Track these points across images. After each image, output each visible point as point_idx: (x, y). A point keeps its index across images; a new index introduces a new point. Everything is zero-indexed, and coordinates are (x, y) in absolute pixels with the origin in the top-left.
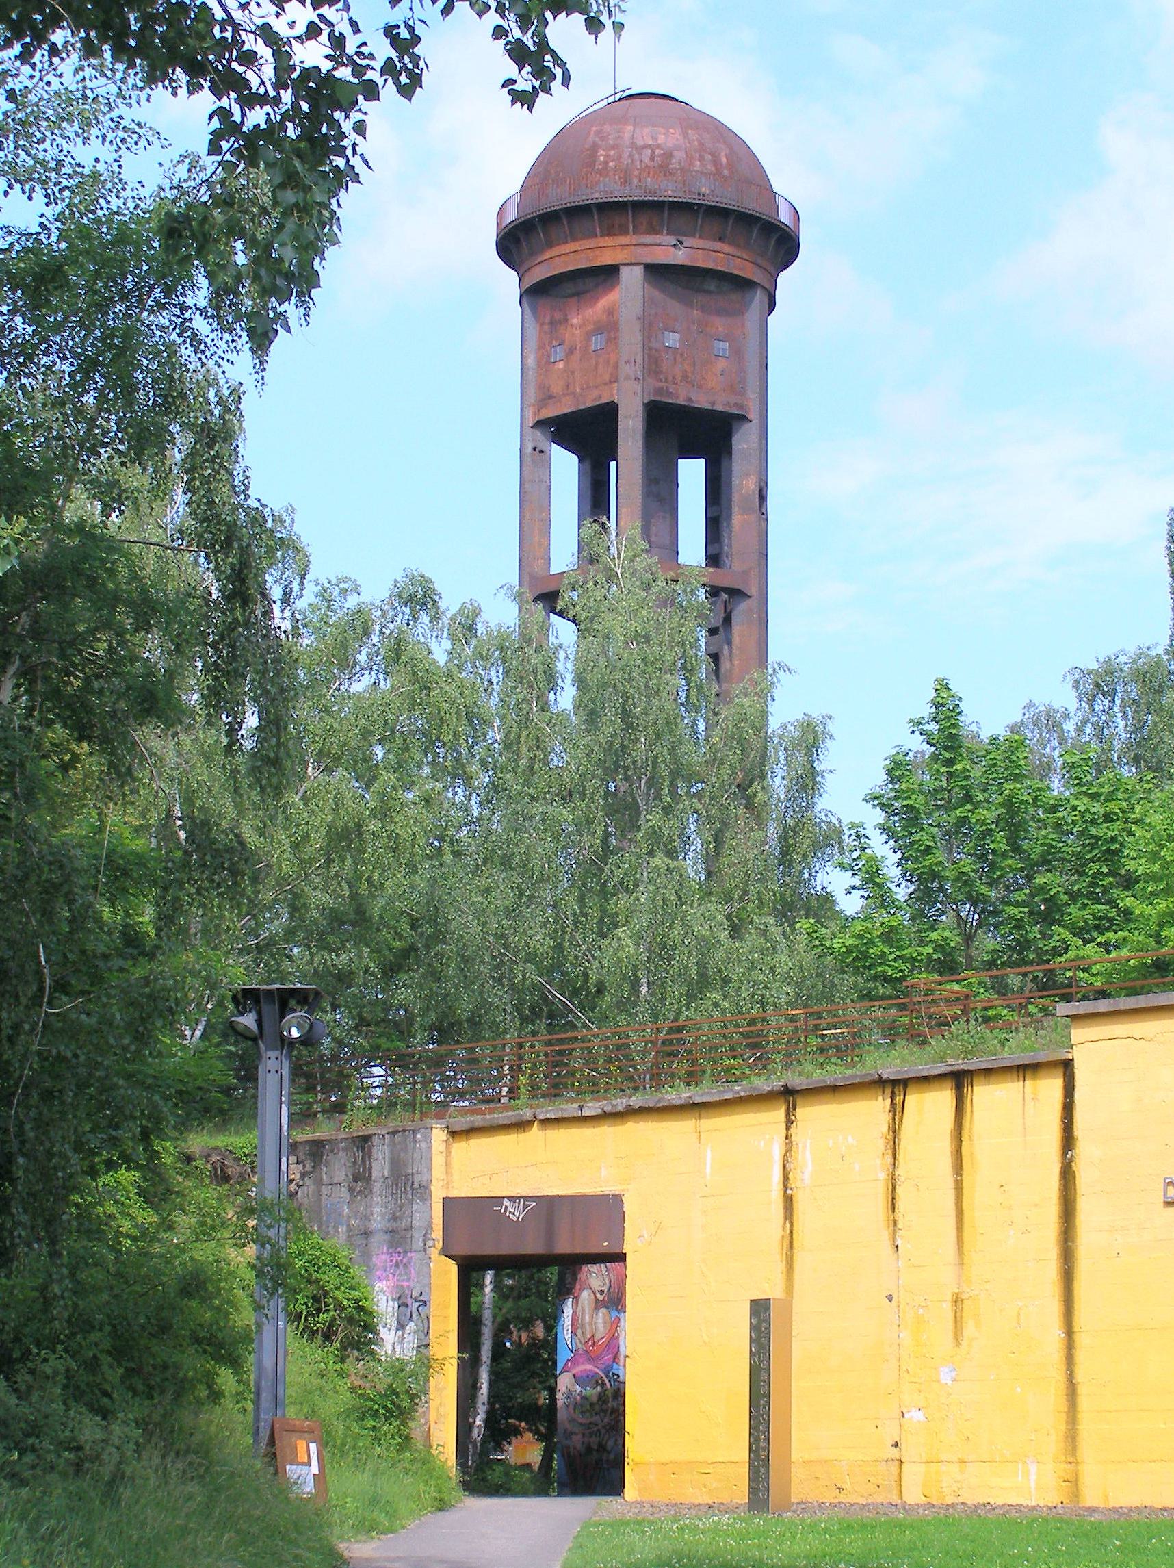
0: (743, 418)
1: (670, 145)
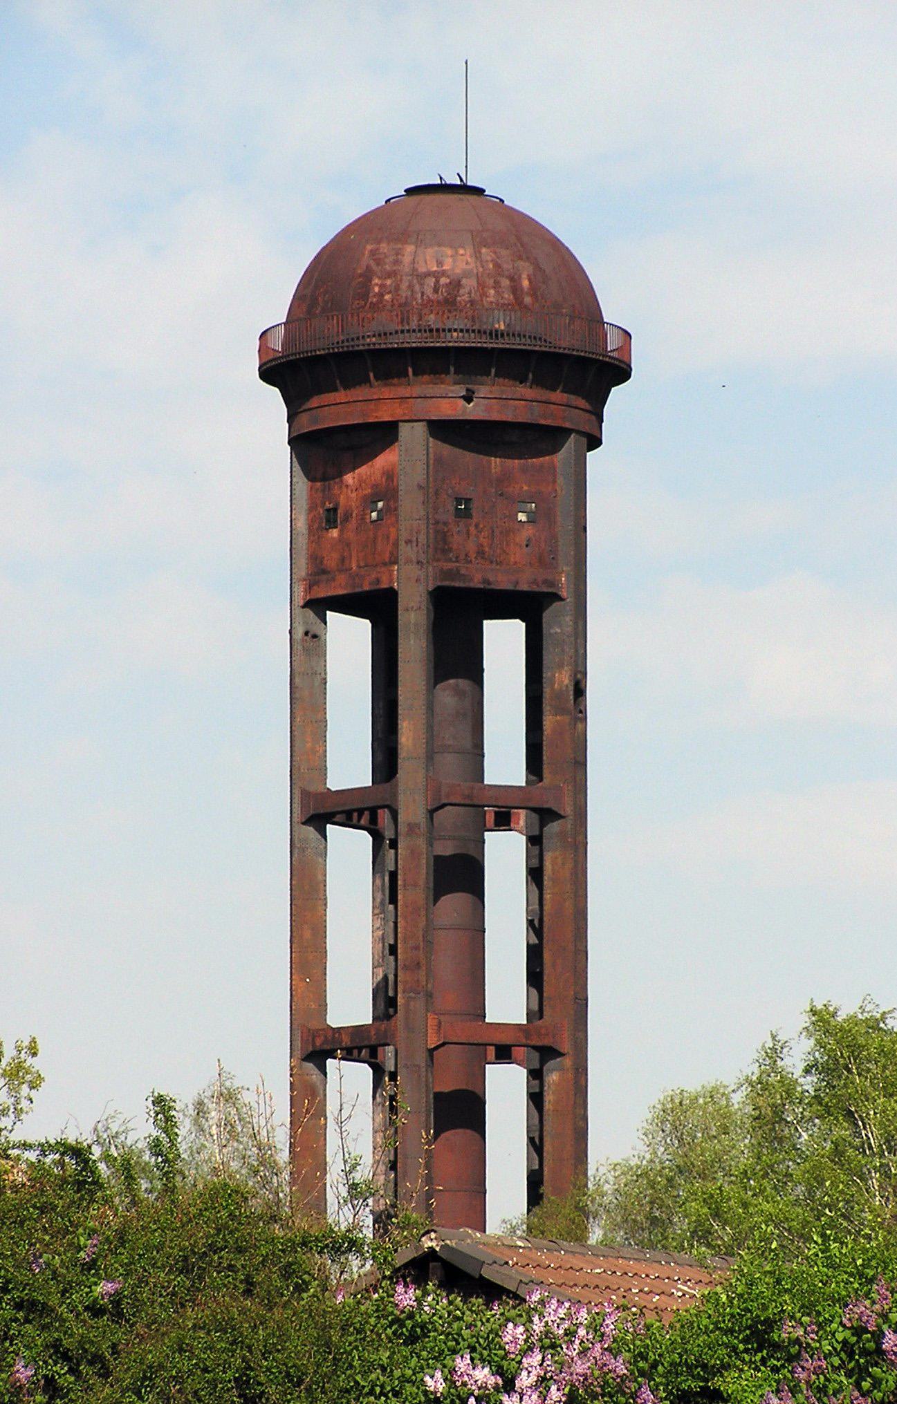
0: (556, 597)
1: (458, 271)
